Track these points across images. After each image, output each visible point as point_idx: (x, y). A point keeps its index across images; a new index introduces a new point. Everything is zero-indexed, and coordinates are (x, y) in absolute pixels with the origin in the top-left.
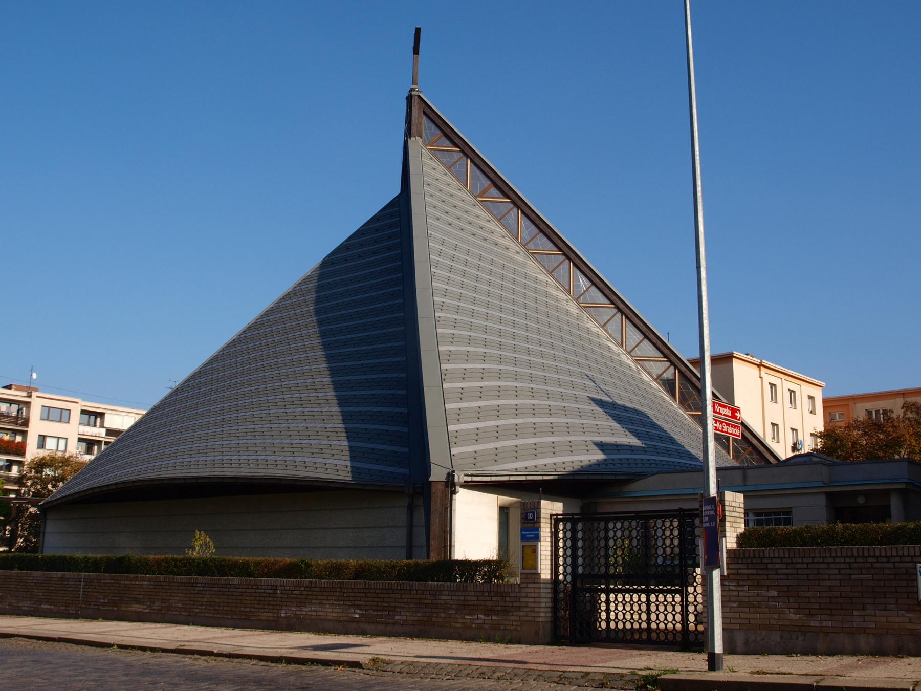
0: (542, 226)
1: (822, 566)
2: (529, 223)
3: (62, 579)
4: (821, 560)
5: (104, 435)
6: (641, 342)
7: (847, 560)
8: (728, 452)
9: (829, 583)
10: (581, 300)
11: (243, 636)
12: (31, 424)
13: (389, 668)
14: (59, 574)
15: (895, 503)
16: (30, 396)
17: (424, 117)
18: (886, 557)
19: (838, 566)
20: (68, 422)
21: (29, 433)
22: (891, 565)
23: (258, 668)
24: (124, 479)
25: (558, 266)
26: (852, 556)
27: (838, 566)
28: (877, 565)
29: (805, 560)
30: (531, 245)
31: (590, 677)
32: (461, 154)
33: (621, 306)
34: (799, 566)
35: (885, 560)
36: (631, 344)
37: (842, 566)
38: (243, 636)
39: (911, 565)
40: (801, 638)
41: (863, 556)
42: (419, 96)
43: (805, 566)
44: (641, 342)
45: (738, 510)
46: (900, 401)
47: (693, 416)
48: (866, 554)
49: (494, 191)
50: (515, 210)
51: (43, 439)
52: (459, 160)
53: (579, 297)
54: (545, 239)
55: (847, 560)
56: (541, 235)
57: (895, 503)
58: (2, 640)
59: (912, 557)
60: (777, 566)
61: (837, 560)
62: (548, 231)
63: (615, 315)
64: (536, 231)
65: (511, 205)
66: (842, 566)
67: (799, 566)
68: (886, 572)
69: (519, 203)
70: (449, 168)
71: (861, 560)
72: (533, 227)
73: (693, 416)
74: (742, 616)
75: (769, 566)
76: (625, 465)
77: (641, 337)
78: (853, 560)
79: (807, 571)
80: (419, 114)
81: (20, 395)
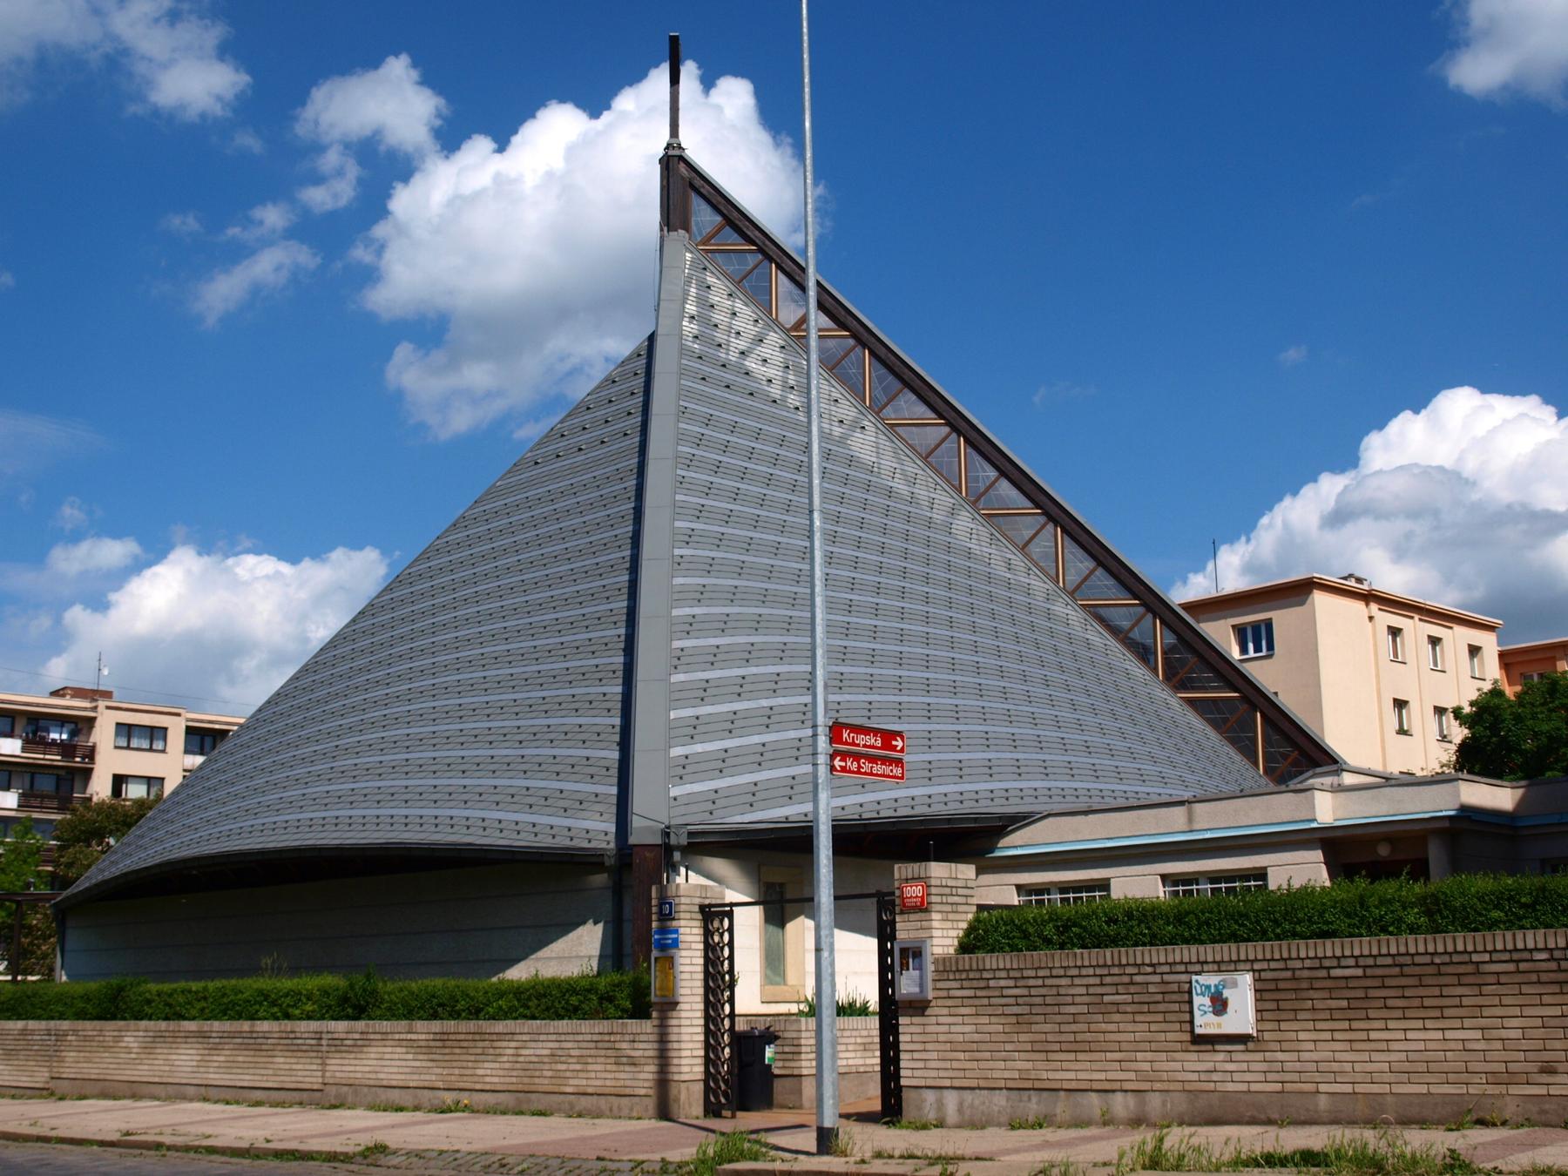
0: (907, 375)
1: (1063, 981)
2: (884, 371)
3: (24, 1032)
4: (1062, 972)
6: (1092, 572)
7: (1098, 971)
8: (1256, 764)
9: (1072, 1009)
10: (981, 504)
12: (98, 758)
14: (20, 1024)
15: (1436, 854)
16: (95, 709)
18: (1151, 965)
19: (1085, 981)
22: (1157, 978)
23: (130, 1162)
26: (1105, 965)
27: (1085, 981)
28: (1138, 979)
29: (1041, 973)
30: (888, 411)
31: (645, 1166)
32: (760, 257)
33: (1054, 511)
34: (1031, 982)
35: (1149, 969)
36: (1073, 579)
37: (1092, 981)
39: (1184, 977)
40: (1034, 1100)
41: (1120, 965)
43: (1040, 982)
45: (938, 899)
47: (1190, 701)
48: (1124, 961)
51: (119, 781)
52: (755, 267)
53: (978, 499)
55: (1098, 971)
57: (1436, 854)
59: (1531, 951)
60: (1003, 983)
61: (1084, 972)
64: (897, 385)
66: (1092, 981)
67: (1031, 982)
68: (1152, 989)
70: (738, 283)
71: (1116, 970)
72: (891, 378)
73: (1190, 701)
75: (992, 983)
78: (1105, 971)
79: (1043, 991)
81: (77, 706)
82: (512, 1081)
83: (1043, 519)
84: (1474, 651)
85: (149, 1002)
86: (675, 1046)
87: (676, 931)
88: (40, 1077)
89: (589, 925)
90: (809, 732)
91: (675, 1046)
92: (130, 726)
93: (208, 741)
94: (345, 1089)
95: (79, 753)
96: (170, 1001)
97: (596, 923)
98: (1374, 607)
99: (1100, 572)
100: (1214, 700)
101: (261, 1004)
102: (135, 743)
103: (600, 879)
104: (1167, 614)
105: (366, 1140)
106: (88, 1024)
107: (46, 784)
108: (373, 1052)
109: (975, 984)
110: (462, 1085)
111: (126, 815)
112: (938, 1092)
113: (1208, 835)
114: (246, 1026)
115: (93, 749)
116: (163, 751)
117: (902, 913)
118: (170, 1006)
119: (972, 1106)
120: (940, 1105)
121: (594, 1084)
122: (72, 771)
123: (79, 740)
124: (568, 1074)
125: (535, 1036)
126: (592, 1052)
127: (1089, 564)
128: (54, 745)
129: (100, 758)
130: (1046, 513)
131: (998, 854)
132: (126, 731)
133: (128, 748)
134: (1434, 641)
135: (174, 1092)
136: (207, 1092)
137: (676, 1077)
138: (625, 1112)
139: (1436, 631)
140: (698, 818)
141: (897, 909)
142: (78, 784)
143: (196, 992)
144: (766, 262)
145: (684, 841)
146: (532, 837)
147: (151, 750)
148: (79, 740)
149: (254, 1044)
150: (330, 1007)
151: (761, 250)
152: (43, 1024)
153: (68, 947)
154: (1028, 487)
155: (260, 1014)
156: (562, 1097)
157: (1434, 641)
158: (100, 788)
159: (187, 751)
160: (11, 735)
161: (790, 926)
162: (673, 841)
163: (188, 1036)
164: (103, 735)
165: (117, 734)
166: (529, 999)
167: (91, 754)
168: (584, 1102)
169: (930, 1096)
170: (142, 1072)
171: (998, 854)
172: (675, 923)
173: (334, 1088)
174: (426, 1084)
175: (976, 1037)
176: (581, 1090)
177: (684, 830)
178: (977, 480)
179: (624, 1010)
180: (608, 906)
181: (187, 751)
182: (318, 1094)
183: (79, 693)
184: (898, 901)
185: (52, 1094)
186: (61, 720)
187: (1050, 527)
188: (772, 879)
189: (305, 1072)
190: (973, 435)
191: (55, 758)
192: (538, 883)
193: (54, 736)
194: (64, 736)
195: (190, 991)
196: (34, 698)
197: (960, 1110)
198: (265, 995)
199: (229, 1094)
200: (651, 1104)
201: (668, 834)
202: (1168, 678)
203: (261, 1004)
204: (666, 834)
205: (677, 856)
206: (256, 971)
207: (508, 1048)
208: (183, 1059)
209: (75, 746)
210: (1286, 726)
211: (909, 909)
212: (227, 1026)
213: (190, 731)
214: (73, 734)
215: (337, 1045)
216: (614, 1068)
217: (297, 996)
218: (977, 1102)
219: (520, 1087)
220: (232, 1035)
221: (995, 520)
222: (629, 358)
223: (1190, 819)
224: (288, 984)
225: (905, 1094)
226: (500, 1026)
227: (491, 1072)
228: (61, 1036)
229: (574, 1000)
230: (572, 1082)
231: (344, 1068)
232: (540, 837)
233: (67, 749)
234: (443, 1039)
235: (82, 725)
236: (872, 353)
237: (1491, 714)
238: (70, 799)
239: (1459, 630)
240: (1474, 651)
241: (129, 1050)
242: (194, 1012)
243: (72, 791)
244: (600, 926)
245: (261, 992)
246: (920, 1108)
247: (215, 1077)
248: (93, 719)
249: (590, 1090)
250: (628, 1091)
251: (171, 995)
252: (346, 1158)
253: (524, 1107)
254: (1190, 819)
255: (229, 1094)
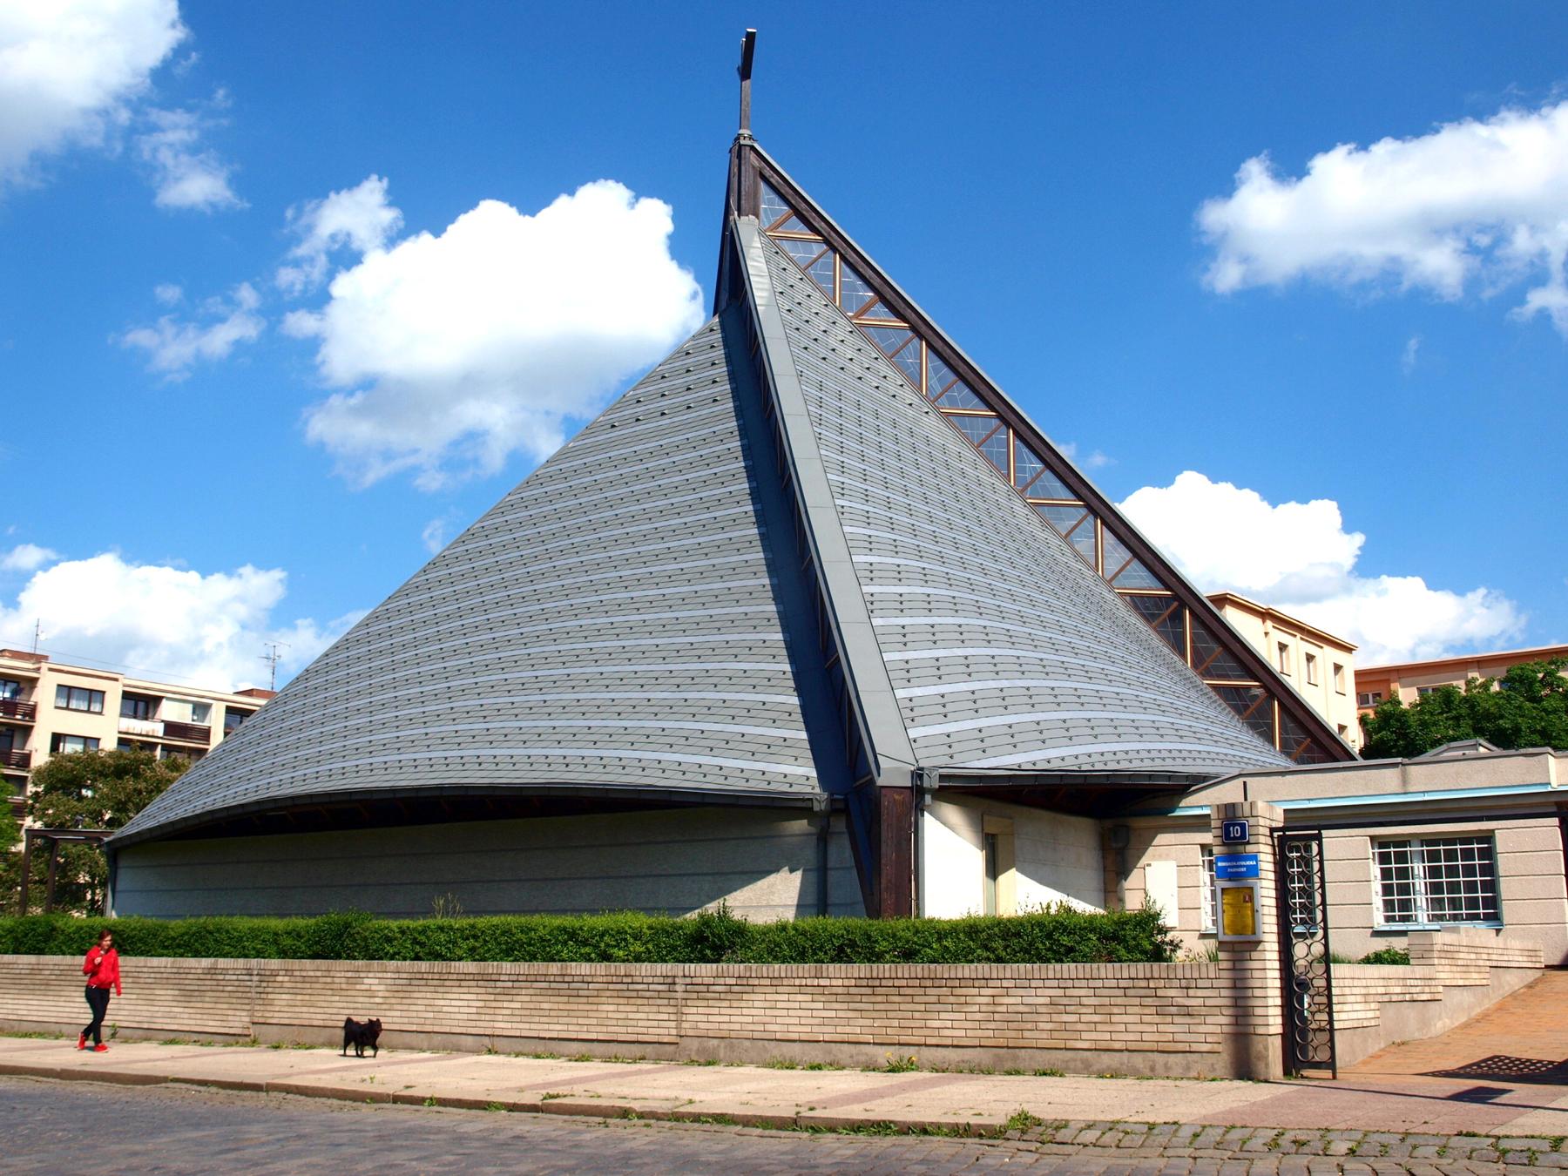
0: (962, 368)
2: (939, 363)
3: (211, 971)
5: (161, 734)
6: (1128, 563)
11: (621, 1075)
12: (39, 716)
14: (206, 962)
17: (762, 185)
25: (989, 436)
38: (45, 1048)
42: (752, 148)
44: (1128, 563)
47: (1214, 687)
50: (916, 341)
51: (57, 739)
54: (967, 391)
56: (960, 383)
58: (5, 1078)
62: (970, 376)
63: (1084, 518)
64: (952, 377)
65: (910, 334)
69: (923, 329)
72: (946, 370)
76: (1189, 761)
77: (1127, 555)
81: (22, 668)
82: (986, 1035)
83: (1084, 511)
84: (1338, 668)
85: (389, 940)
86: (1257, 993)
87: (1255, 857)
88: (238, 1021)
91: (1257, 993)
92: (70, 688)
93: (141, 705)
94: (715, 1042)
95: (20, 711)
96: (423, 939)
97: (792, 871)
98: (1269, 623)
99: (1136, 564)
100: (1237, 688)
101: (565, 943)
102: (73, 705)
103: (800, 826)
106: (307, 963)
108: (758, 999)
110: (904, 1039)
111: (103, 764)
113: (1427, 797)
114: (554, 968)
116: (100, 713)
118: (422, 945)
121: (1121, 1039)
123: (20, 699)
124: (1080, 1027)
125: (1025, 982)
129: (41, 716)
131: (1178, 813)
132: (66, 692)
133: (67, 708)
134: (1310, 658)
135: (449, 1043)
136: (491, 1044)
137: (1260, 1030)
138: (1160, 1069)
139: (1313, 650)
140: (935, 760)
142: (17, 740)
143: (461, 930)
144: (830, 253)
145: (936, 785)
146: (721, 780)
147: (88, 711)
148: (20, 699)
149: (571, 990)
150: (674, 948)
151: (827, 241)
152: (241, 963)
153: (119, 887)
156: (1070, 1054)
157: (1310, 658)
159: (123, 715)
161: (1002, 878)
163: (462, 979)
164: (44, 695)
165: (58, 695)
166: (990, 938)
167: (31, 713)
168: (1107, 1060)
171: (1178, 813)
172: (1249, 848)
173: (696, 1042)
174: (852, 1038)
177: (936, 773)
178: (1023, 470)
180: (810, 854)
181: (123, 715)
182: (673, 1048)
185: (254, 1042)
187: (1091, 518)
188: (991, 830)
189: (653, 1021)
190: (1021, 428)
192: (732, 824)
194: (7, 695)
195: (451, 928)
198: (572, 935)
200: (1223, 1061)
201: (921, 777)
202: (1195, 665)
203: (565, 943)
204: (918, 774)
205: (928, 798)
206: (429, 912)
207: (982, 997)
208: (457, 1000)
209: (16, 705)
210: (1300, 714)
212: (523, 967)
213: (127, 696)
214: (15, 693)
215: (700, 991)
217: (620, 936)
220: (532, 979)
221: (1039, 509)
222: (700, 334)
223: (1405, 782)
227: (949, 1024)
228: (267, 977)
230: (1085, 1036)
231: (702, 1018)
232: (730, 781)
234: (873, 986)
237: (1398, 720)
240: (1338, 668)
241: (371, 994)
243: (11, 747)
244: (798, 875)
245: (564, 930)
247: (502, 1027)
248: (35, 680)
249: (1117, 1046)
251: (423, 932)
254: (1405, 782)
255: (540, 1047)
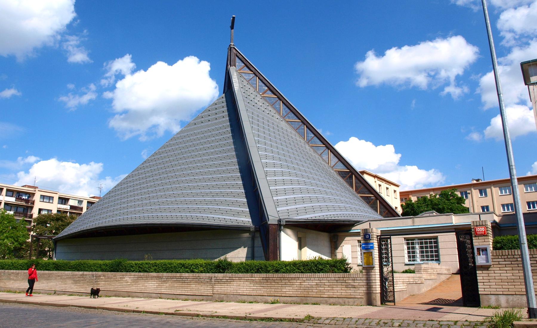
0: (292, 108)
12: (35, 204)
13: (319, 321)
14: (81, 273)
20: (522, 64)
21: (34, 208)
24: (101, 225)
31: (336, 319)
36: (333, 164)
46: (439, 192)
47: (361, 196)
48: (513, 254)
49: (269, 92)
50: (279, 101)
51: (40, 210)
62: (294, 111)
69: (281, 98)
72: (287, 109)
74: (504, 287)
80: (232, 56)
81: (31, 190)
82: (299, 293)
83: (325, 148)
84: (395, 191)
85: (132, 267)
86: (373, 281)
89: (242, 248)
90: (275, 198)
91: (373, 281)
93: (64, 201)
95: (30, 202)
96: (141, 266)
98: (376, 179)
99: (339, 162)
101: (181, 268)
103: (247, 235)
104: (356, 174)
105: (306, 314)
107: (21, 210)
109: (511, 260)
110: (276, 295)
112: (496, 296)
114: (178, 275)
115: (34, 201)
117: (475, 236)
119: (513, 300)
120: (497, 300)
121: (336, 294)
122: (28, 207)
124: (324, 291)
125: (309, 279)
126: (335, 284)
127: (337, 160)
128: (23, 200)
130: (326, 146)
132: (43, 197)
135: (149, 296)
136: (160, 296)
137: (374, 292)
138: (346, 303)
139: (388, 186)
140: (284, 217)
141: (473, 235)
142: (29, 211)
143: (152, 264)
149: (183, 281)
150: (212, 269)
151: (254, 74)
154: (322, 139)
155: (181, 271)
157: (387, 188)
158: (35, 213)
159: (58, 203)
160: (12, 196)
162: (282, 223)
163: (152, 277)
164: (37, 198)
167: (33, 203)
168: (332, 300)
169: (493, 298)
170: (133, 289)
172: (371, 241)
173: (218, 295)
174: (261, 294)
175: (513, 277)
176: (331, 296)
178: (308, 137)
179: (342, 270)
180: (250, 243)
181: (58, 203)
183: (29, 187)
184: (473, 233)
186: (26, 193)
187: (327, 150)
189: (206, 290)
191: (23, 203)
192: (227, 235)
193: (24, 197)
196: (17, 186)
197: (507, 302)
199: (251, 299)
200: (364, 301)
201: (280, 221)
202: (356, 190)
203: (181, 268)
204: (280, 221)
205: (282, 227)
206: (143, 259)
209: (29, 201)
210: (385, 204)
211: (477, 235)
212: (170, 274)
213: (60, 198)
214: (29, 197)
215: (219, 281)
216: (346, 289)
218: (515, 299)
219: (303, 295)
223: (413, 223)
224: (191, 262)
225: (481, 297)
226: (293, 275)
227: (288, 290)
228: (98, 277)
229: (320, 267)
231: (220, 289)
233: (27, 201)
234: (267, 280)
235: (31, 195)
236: (283, 102)
238: (27, 214)
239: (392, 186)
242: (152, 270)
244: (246, 249)
246: (488, 301)
247: (163, 291)
249: (335, 296)
250: (352, 296)
252: (301, 321)
253: (308, 302)
254: (413, 223)
255: (174, 297)
